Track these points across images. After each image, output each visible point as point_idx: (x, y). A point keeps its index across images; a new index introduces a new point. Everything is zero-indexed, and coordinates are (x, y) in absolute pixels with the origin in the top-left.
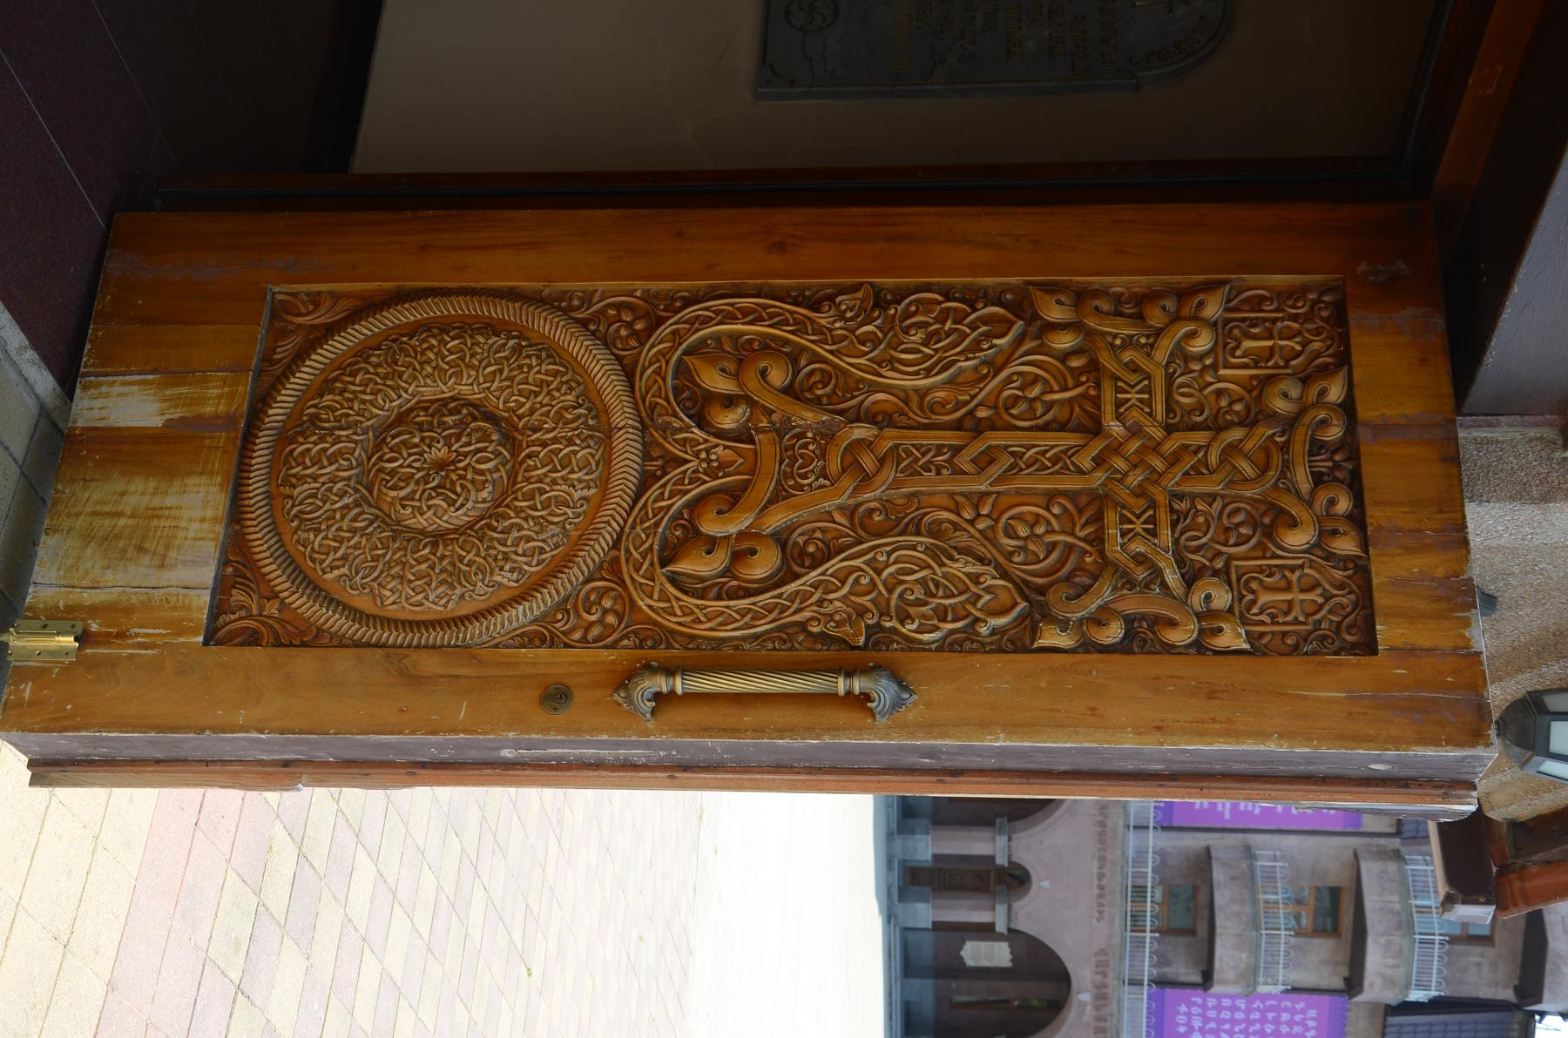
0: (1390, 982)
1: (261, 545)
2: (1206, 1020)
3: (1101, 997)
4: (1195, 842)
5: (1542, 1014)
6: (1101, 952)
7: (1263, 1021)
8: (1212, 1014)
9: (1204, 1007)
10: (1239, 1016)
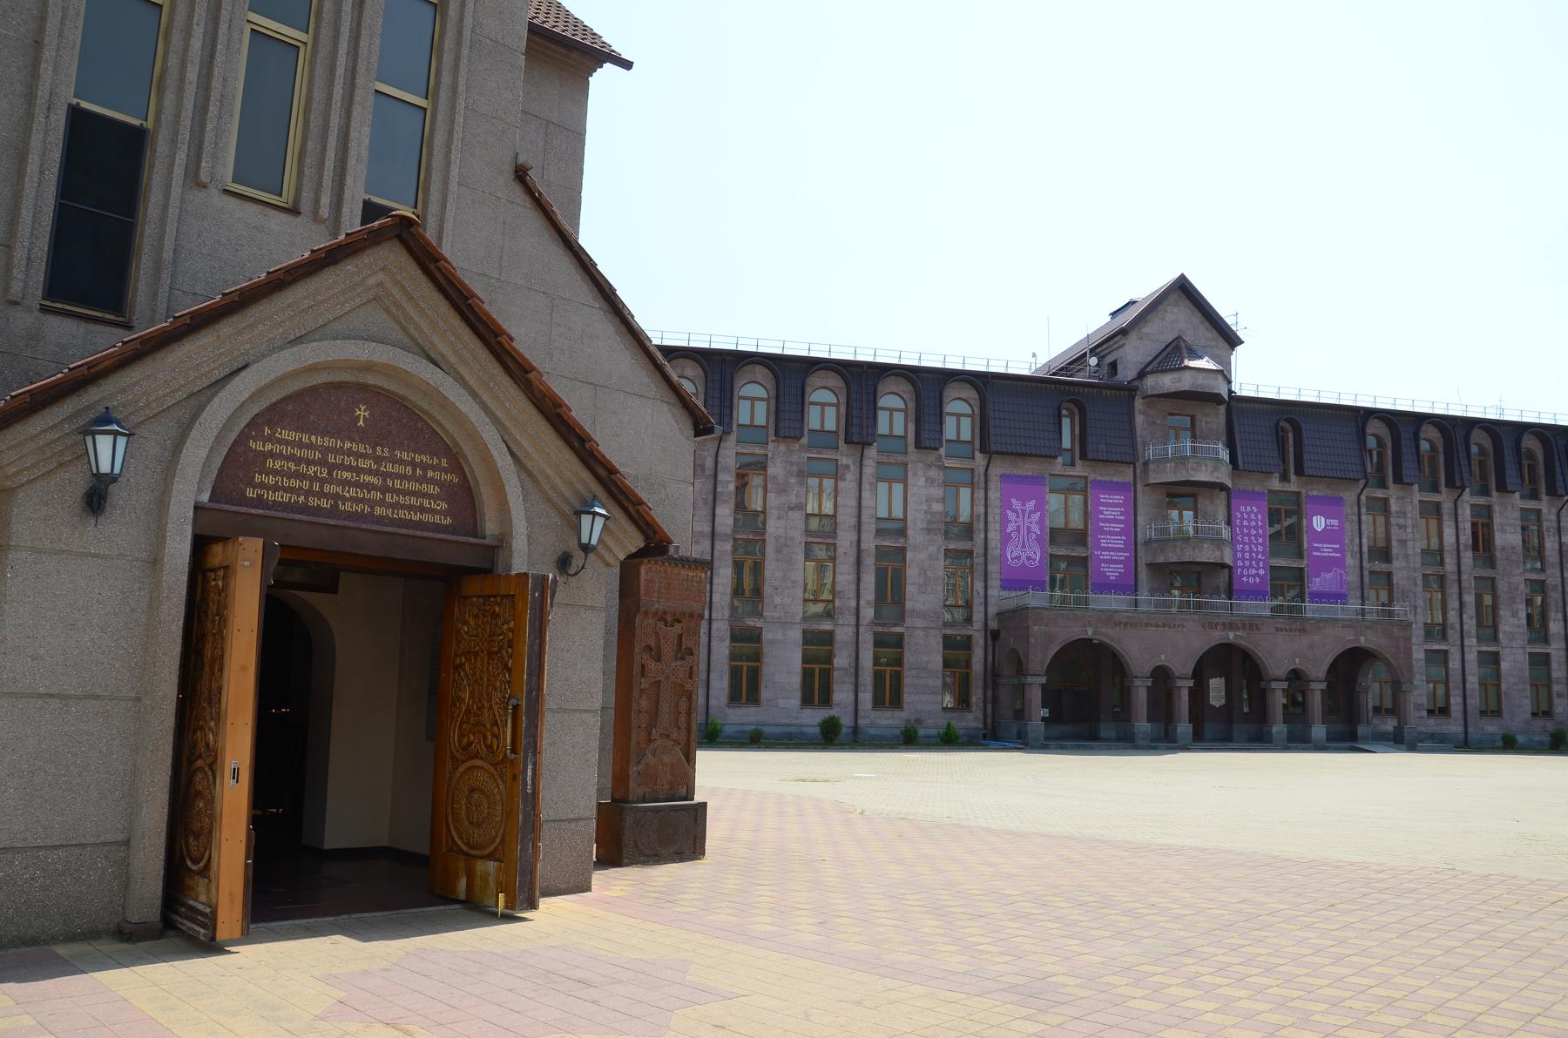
0: (1216, 469)
1: (487, 851)
2: (1251, 566)
3: (1231, 626)
4: (1143, 574)
5: (1230, 392)
6: (1203, 626)
7: (1249, 535)
8: (1247, 563)
9: (1243, 567)
10: (1247, 548)
